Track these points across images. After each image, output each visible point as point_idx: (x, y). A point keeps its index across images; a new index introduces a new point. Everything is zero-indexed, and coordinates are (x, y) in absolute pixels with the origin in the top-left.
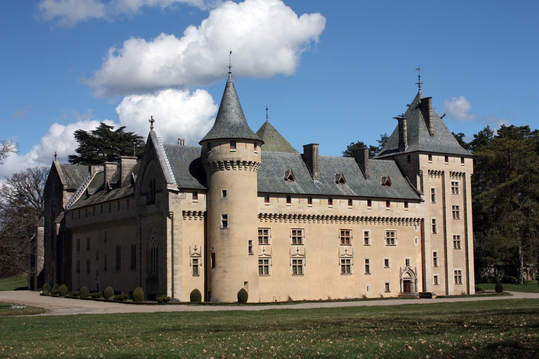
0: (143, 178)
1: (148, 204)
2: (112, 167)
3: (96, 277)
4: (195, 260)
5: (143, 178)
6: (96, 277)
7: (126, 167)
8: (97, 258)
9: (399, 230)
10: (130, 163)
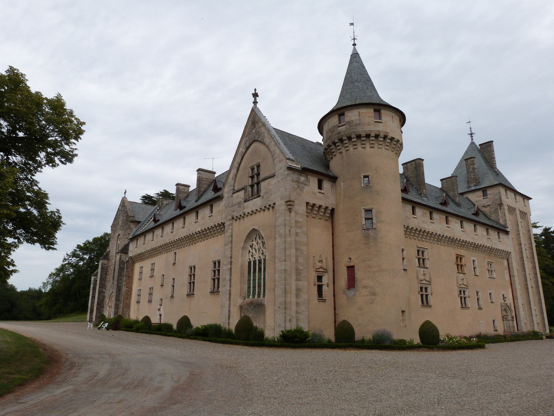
0: (238, 170)
1: (245, 201)
2: (184, 189)
3: (159, 307)
4: (320, 278)
5: (238, 170)
6: (159, 307)
7: (204, 181)
8: (162, 285)
9: (469, 257)
10: (208, 177)
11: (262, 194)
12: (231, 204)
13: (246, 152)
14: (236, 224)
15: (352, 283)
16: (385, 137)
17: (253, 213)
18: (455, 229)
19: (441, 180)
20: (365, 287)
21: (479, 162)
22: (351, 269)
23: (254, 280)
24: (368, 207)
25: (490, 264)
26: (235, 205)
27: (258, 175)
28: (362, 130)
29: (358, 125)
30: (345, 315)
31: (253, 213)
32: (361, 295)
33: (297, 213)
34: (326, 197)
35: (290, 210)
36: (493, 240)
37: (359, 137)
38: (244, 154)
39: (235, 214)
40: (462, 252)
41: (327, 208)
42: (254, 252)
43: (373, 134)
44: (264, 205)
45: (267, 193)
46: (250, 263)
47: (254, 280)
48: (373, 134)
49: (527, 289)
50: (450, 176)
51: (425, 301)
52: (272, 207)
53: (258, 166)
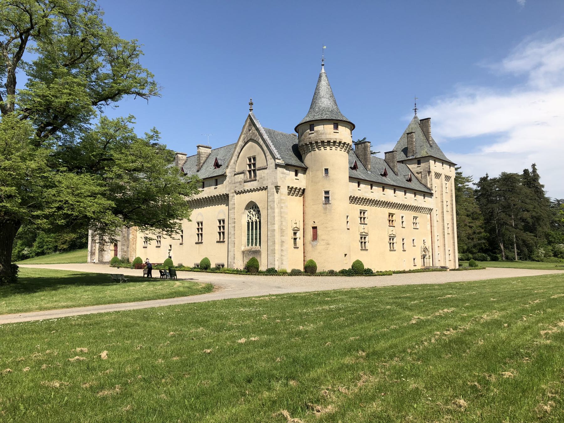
9: (398, 213)
11: (257, 178)
12: (233, 182)
13: (244, 146)
14: (237, 197)
15: (315, 237)
16: (340, 143)
17: (251, 191)
18: (389, 195)
19: (386, 153)
20: (323, 240)
21: (418, 136)
22: (315, 228)
23: (252, 234)
24: (327, 190)
25: (415, 218)
26: (237, 183)
27: (254, 165)
28: (325, 138)
29: (321, 134)
30: (313, 256)
31: (251, 191)
32: (320, 244)
33: (282, 194)
34: (301, 181)
35: (277, 192)
36: (420, 201)
37: (323, 142)
38: (243, 147)
39: (237, 190)
40: (392, 211)
41: (300, 188)
42: (251, 216)
43: (332, 141)
44: (259, 186)
45: (261, 178)
46: (248, 223)
47: (252, 234)
48: (332, 141)
49: (444, 235)
50: (391, 150)
51: (364, 247)
52: (265, 189)
53: (254, 159)
